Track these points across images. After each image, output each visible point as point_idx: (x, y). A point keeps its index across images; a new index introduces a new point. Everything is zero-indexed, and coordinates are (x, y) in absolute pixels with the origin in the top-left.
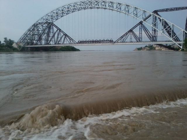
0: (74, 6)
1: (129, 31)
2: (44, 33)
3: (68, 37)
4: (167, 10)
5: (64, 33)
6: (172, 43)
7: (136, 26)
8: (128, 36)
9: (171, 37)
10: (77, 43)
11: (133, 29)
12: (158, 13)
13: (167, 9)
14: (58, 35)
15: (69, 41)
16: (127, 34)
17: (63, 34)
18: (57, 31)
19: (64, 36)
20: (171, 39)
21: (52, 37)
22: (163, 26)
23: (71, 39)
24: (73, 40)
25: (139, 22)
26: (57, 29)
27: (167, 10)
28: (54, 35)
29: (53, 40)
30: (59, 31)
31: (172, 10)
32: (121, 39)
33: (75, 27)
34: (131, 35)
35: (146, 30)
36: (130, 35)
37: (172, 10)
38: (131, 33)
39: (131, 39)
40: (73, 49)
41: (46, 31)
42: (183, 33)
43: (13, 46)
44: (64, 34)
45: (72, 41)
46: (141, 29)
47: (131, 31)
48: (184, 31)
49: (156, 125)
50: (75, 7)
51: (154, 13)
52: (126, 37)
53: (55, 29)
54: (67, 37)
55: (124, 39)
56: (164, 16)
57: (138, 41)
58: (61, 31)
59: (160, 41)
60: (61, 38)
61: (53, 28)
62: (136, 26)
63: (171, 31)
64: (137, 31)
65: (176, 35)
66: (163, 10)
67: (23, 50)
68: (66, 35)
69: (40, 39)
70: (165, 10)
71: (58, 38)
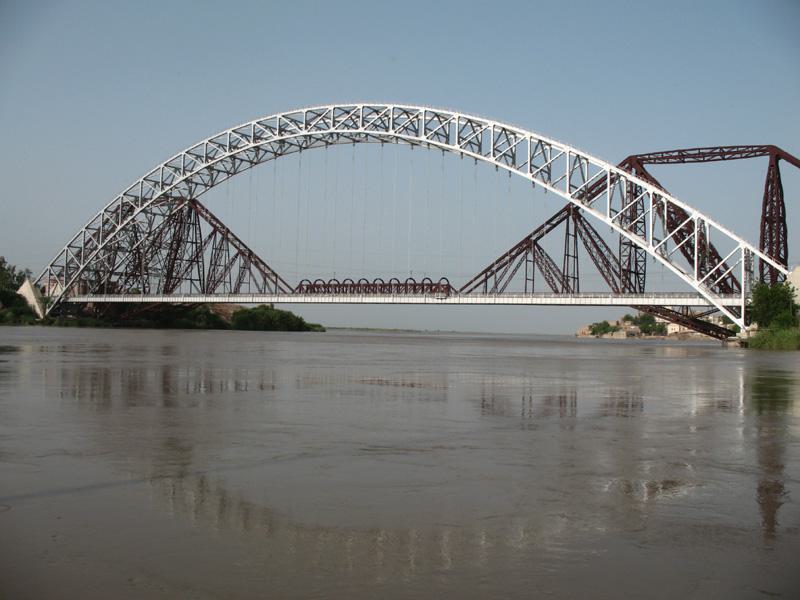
0: (282, 130)
1: (520, 244)
2: (156, 245)
3: (256, 265)
4: (681, 157)
5: (242, 248)
6: (702, 302)
7: (551, 224)
8: (515, 270)
9: (691, 262)
10: (293, 292)
11: (539, 238)
12: (647, 167)
13: (680, 151)
14: (218, 250)
15: (260, 281)
16: (510, 256)
17: (236, 251)
18: (210, 237)
19: (240, 261)
20: (696, 284)
21: (191, 261)
22: (662, 216)
23: (269, 274)
24: (276, 276)
25: (564, 206)
26: (212, 229)
27: (681, 157)
28: (200, 250)
29: (195, 274)
30: (219, 236)
31: (701, 156)
32: (485, 280)
33: (290, 223)
34: (530, 264)
35: (593, 241)
36: (525, 267)
37: (701, 156)
38: (530, 257)
39: (530, 283)
40: (289, 323)
41: (168, 238)
42: (762, 269)
43: (18, 292)
44: (241, 253)
45: (276, 283)
46: (572, 239)
47: (529, 244)
48: (749, 256)
49: (646, 495)
50: (286, 136)
51: (629, 170)
52: (506, 271)
53: (206, 229)
54: (253, 268)
55: (498, 277)
56: (677, 187)
57: (559, 287)
58: (230, 236)
59: (658, 295)
60: (227, 268)
61: (196, 224)
62: (551, 224)
63: (707, 273)
64: (553, 244)
65: (720, 259)
66: (668, 158)
67: (64, 314)
68: (249, 256)
69: (138, 269)
70: (671, 157)
71: (214, 264)
